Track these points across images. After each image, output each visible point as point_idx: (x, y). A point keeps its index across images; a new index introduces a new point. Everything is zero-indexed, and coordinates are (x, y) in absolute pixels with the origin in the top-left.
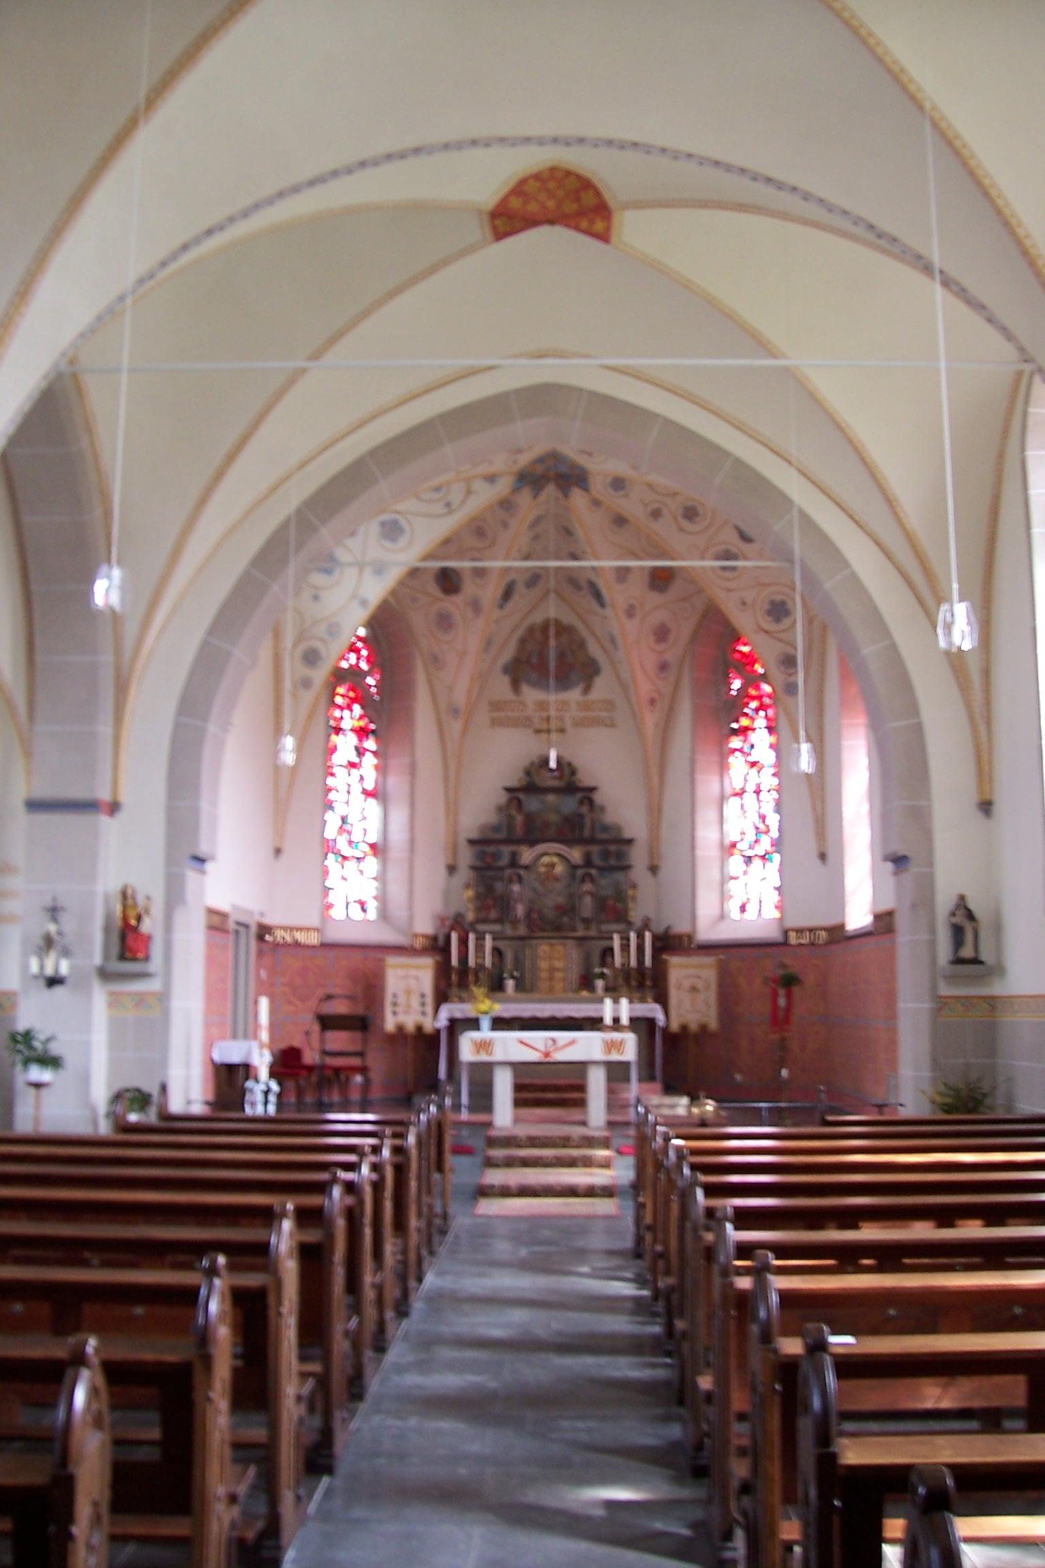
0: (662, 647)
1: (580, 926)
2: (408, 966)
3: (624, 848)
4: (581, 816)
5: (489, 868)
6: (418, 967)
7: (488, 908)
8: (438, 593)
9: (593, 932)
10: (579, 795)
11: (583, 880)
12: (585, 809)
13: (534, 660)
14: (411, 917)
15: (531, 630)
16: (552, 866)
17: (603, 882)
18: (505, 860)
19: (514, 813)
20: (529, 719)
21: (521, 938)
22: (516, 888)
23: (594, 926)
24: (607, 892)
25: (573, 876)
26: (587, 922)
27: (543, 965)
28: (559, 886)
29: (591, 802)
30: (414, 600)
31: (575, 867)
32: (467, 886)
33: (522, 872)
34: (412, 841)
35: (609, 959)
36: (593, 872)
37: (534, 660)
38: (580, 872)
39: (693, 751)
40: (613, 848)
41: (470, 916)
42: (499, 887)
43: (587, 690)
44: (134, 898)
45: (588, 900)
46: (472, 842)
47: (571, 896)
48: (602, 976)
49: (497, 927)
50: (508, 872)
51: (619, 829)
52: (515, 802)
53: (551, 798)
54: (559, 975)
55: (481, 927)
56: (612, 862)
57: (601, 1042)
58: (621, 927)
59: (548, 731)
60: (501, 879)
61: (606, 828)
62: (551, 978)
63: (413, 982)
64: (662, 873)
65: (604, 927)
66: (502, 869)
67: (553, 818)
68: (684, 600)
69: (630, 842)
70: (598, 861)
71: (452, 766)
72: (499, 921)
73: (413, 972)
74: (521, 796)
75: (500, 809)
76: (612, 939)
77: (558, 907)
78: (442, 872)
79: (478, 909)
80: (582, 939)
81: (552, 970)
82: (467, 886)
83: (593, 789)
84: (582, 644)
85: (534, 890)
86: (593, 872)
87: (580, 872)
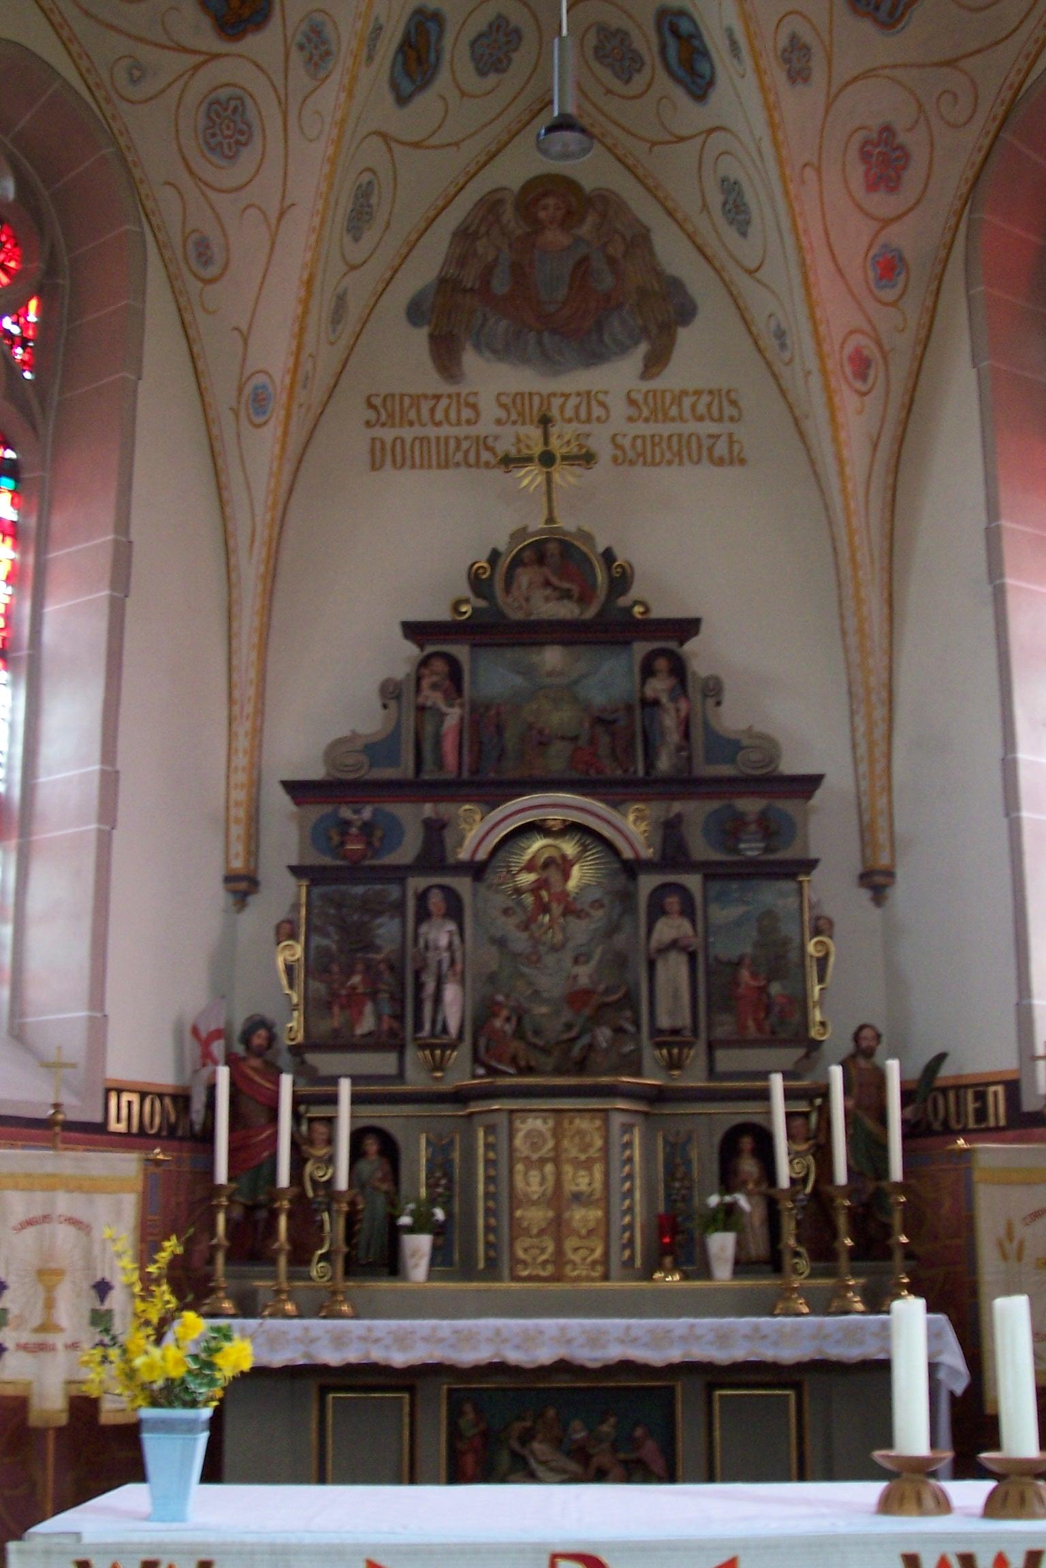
0: (883, 204)
1: (651, 1055)
2: (51, 1183)
3: (788, 806)
4: (651, 705)
5: (354, 871)
6: (85, 1186)
7: (353, 1003)
8: (210, 41)
9: (694, 1078)
10: (641, 649)
11: (657, 910)
12: (659, 686)
13: (501, 285)
14: (98, 1028)
15: (491, 205)
16: (564, 866)
17: (722, 914)
18: (408, 850)
19: (433, 698)
20: (483, 443)
21: (460, 1097)
22: (440, 934)
23: (696, 1056)
24: (741, 946)
25: (626, 898)
26: (669, 1039)
27: (532, 1183)
28: (580, 930)
29: (679, 669)
30: (138, 72)
31: (632, 869)
32: (286, 931)
33: (463, 885)
34: (109, 782)
35: (749, 1166)
36: (693, 882)
37: (501, 285)
38: (647, 883)
39: (993, 510)
40: (750, 806)
41: (294, 1027)
42: (387, 931)
43: (656, 362)
44: (1038, 1501)
45: (674, 970)
46: (298, 790)
47: (621, 961)
48: (728, 1217)
49: (384, 1063)
50: (417, 883)
51: (769, 747)
52: (439, 666)
53: (552, 657)
54: (583, 1217)
55: (323, 1062)
56: (751, 849)
57: (956, 1557)
58: (791, 1055)
59: (547, 459)
60: (399, 908)
61: (726, 747)
62: (558, 1228)
63: (64, 1236)
64: (900, 892)
65: (727, 1059)
66: (398, 874)
67: (560, 718)
68: (950, 63)
69: (808, 784)
70: (700, 848)
71: (250, 570)
72: (389, 1041)
73: (64, 1203)
74: (461, 652)
75: (390, 692)
76: (764, 1095)
77: (577, 998)
78: (215, 893)
79: (314, 1007)
80: (658, 1096)
81: (558, 1199)
82: (286, 931)
83: (688, 628)
84: (640, 240)
85: (501, 943)
86: (693, 882)
87: (647, 883)
